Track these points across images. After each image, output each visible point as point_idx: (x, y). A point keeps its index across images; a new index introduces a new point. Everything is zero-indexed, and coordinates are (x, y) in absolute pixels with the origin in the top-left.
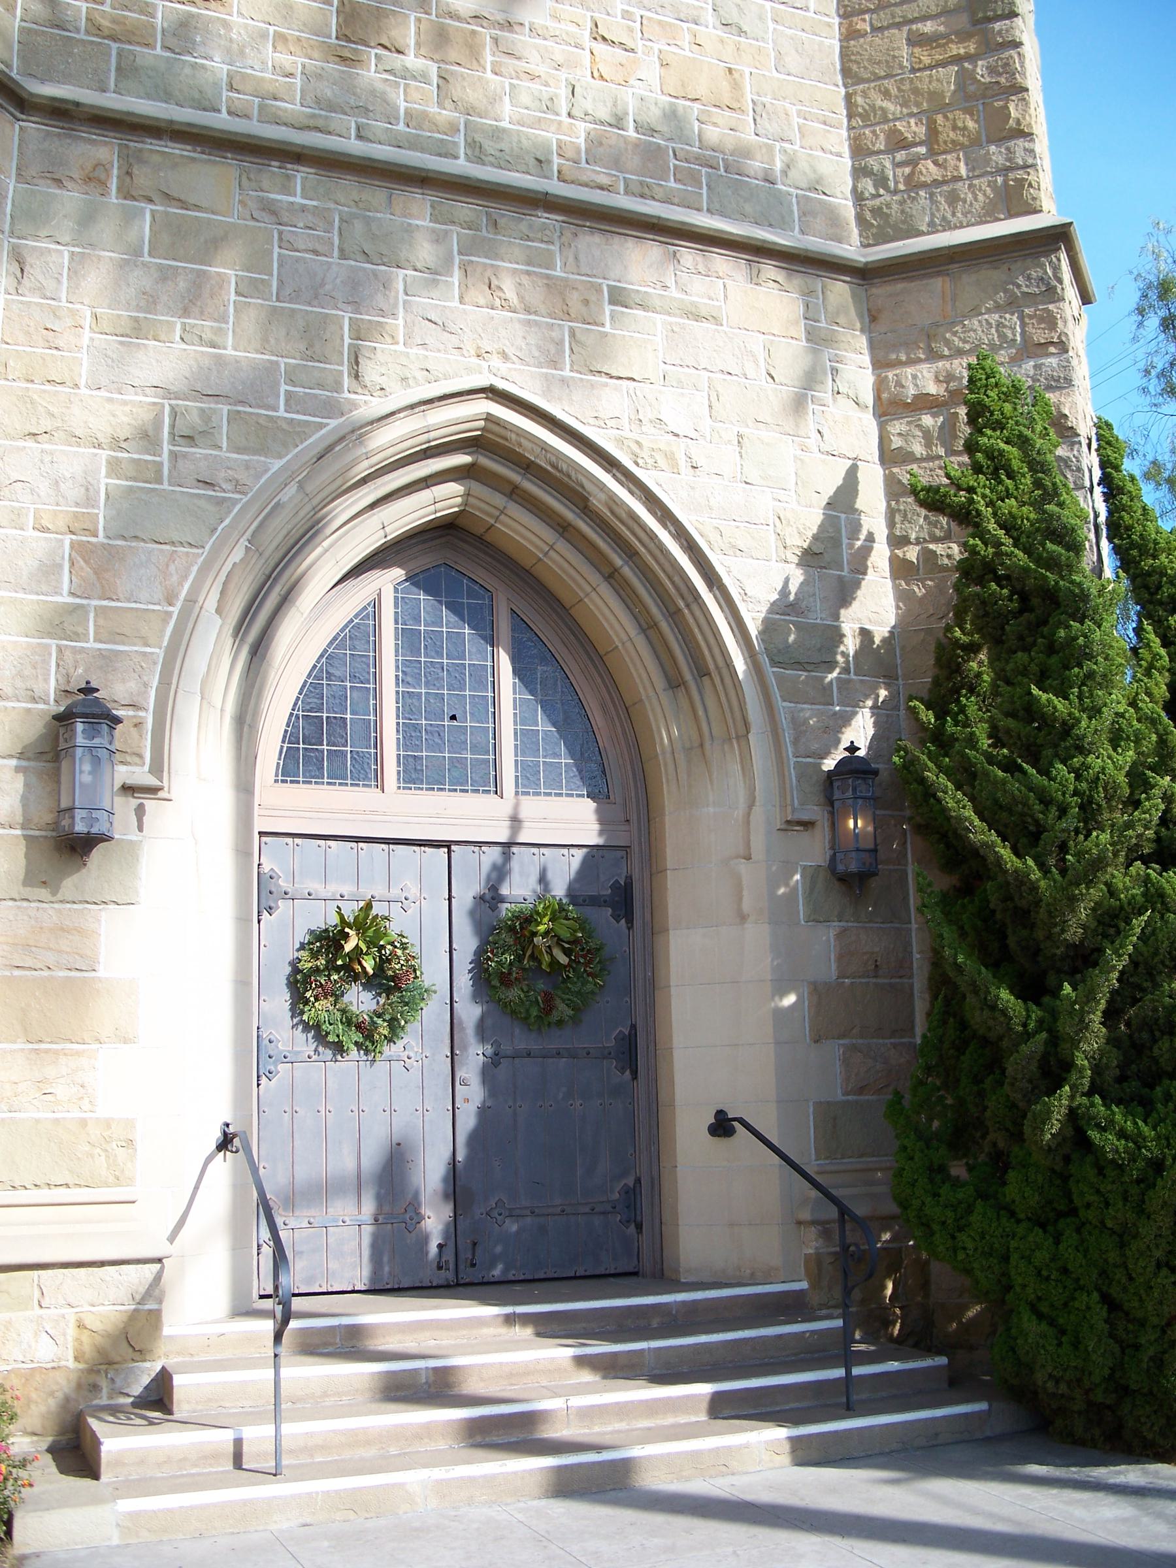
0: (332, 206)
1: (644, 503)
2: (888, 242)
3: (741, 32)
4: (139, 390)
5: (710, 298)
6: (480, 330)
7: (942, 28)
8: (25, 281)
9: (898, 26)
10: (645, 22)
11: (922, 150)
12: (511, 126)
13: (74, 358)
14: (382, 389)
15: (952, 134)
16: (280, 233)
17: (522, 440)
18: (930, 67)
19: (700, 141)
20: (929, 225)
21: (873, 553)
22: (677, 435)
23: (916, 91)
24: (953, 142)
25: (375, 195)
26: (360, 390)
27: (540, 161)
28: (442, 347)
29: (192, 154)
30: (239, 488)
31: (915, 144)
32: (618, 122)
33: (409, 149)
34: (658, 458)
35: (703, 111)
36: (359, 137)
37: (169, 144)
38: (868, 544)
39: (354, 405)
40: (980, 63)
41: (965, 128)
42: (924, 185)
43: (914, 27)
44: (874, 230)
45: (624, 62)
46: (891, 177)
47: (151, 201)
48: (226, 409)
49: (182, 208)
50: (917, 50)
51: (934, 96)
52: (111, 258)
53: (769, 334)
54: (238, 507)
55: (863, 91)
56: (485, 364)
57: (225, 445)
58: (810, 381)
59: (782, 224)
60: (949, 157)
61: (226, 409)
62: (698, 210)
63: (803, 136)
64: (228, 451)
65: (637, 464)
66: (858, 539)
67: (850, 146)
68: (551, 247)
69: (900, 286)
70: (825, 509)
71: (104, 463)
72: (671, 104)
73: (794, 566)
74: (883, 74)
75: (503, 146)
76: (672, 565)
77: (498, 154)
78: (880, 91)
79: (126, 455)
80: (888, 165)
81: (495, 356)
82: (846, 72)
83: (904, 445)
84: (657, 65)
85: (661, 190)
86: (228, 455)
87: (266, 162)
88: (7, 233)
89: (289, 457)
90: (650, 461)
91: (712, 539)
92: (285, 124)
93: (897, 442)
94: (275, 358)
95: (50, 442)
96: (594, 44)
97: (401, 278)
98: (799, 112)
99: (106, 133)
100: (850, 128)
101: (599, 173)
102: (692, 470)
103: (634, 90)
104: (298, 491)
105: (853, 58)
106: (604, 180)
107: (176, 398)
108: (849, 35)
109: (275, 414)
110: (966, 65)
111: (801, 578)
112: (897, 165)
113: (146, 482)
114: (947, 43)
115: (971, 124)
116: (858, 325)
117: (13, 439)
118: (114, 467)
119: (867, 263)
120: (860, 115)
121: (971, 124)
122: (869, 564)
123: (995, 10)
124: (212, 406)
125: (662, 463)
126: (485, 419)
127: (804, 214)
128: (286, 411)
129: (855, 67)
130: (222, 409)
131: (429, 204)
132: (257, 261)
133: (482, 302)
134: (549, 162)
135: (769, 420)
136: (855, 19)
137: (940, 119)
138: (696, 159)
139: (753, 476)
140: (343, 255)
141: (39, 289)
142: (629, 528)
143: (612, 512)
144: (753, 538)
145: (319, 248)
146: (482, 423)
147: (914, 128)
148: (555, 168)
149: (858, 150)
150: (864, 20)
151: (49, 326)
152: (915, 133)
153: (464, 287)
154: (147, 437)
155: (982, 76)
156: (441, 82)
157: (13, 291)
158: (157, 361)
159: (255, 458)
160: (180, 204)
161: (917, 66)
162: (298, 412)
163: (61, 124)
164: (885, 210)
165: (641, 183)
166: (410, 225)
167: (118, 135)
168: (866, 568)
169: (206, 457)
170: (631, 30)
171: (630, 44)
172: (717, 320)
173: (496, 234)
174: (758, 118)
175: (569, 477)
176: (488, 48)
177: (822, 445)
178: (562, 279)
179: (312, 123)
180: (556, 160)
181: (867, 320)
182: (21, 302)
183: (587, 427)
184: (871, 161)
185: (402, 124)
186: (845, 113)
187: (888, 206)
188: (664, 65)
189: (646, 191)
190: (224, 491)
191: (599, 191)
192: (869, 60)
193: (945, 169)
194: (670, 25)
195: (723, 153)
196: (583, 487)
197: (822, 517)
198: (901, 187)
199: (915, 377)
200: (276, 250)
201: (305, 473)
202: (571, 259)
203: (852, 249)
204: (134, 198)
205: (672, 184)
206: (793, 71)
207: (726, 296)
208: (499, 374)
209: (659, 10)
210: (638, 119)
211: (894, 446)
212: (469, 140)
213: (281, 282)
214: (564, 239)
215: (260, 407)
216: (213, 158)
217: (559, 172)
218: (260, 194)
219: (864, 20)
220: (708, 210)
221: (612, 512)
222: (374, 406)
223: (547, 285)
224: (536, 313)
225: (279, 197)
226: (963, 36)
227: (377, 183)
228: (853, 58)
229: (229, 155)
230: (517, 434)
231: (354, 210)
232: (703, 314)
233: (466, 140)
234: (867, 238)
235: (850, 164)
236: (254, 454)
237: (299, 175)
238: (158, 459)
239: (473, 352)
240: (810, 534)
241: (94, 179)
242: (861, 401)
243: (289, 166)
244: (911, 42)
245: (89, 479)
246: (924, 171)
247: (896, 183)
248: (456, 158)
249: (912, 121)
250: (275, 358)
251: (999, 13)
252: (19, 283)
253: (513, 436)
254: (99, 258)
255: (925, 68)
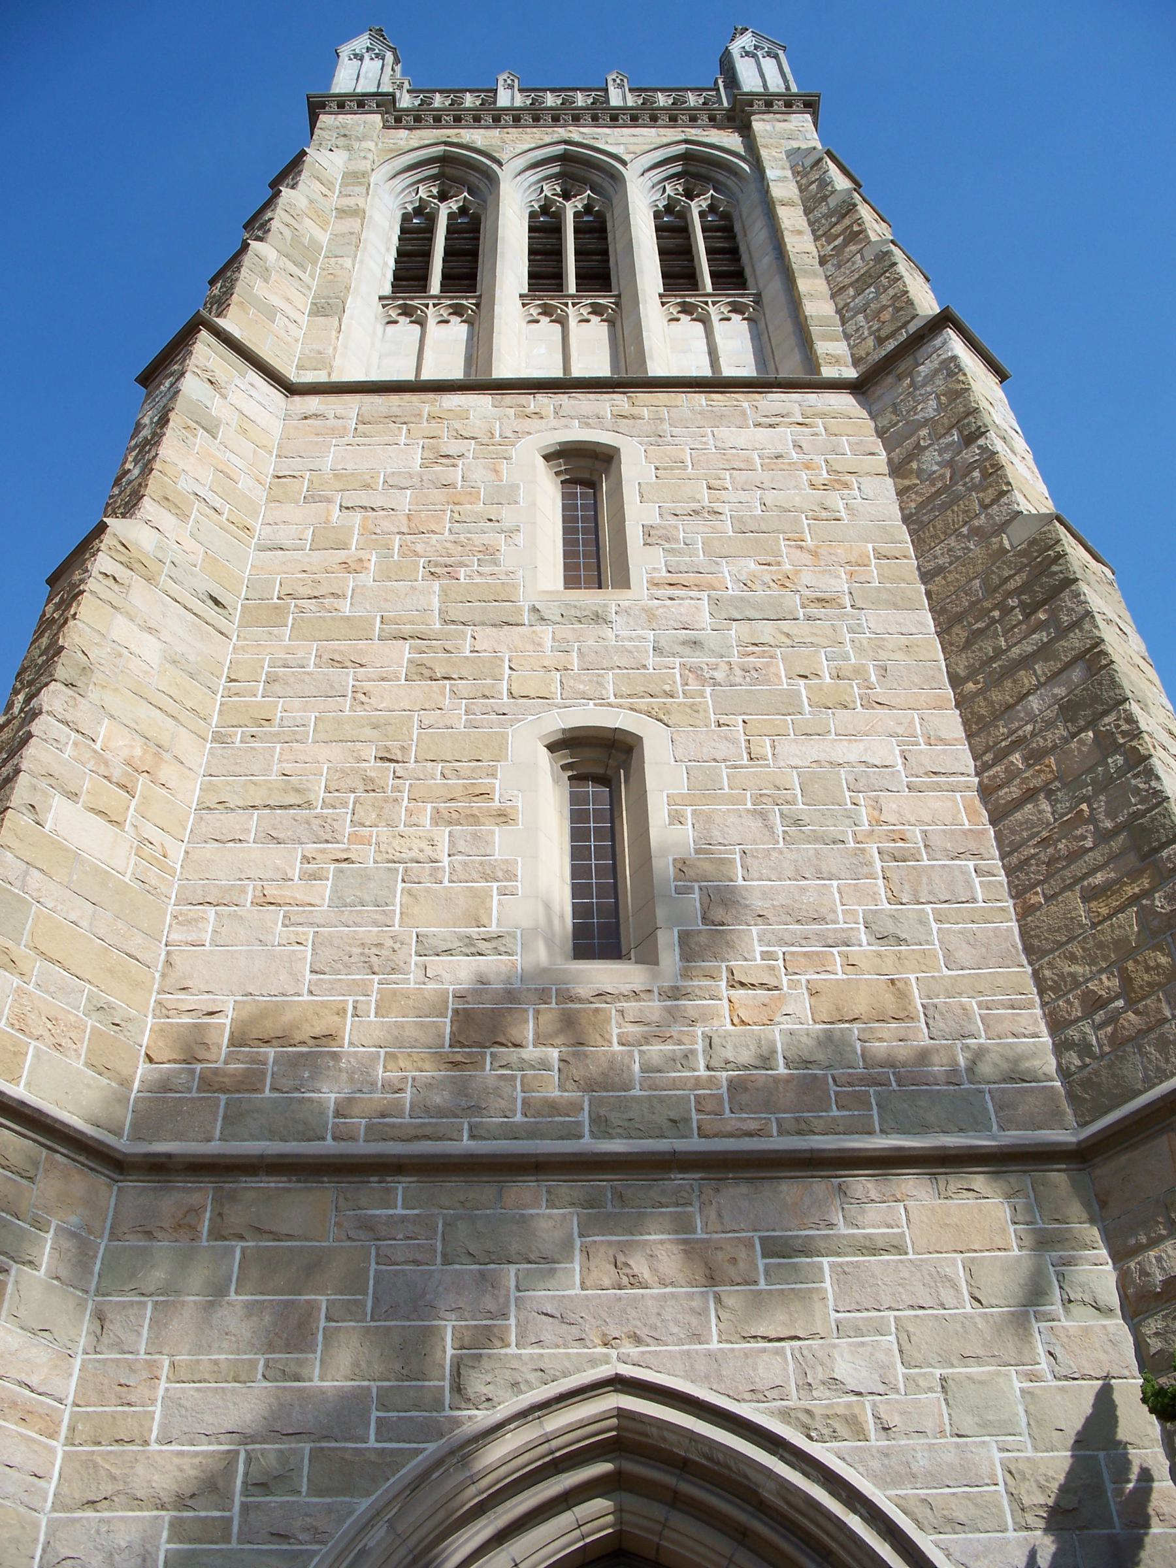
0: (436, 1211)
1: (823, 1486)
2: (1106, 1113)
3: (900, 941)
4: (213, 1439)
5: (889, 1226)
6: (604, 1315)
7: (1112, 875)
8: (105, 1339)
9: (1070, 887)
10: (787, 957)
11: (1120, 1003)
12: (643, 1093)
13: (146, 1412)
14: (489, 1400)
15: (1146, 977)
16: (378, 1248)
17: (666, 1434)
18: (1110, 917)
19: (864, 1060)
20: (1144, 1082)
21: (1154, 1495)
22: (859, 1394)
23: (1100, 945)
24: (1149, 984)
25: (482, 1191)
26: (463, 1405)
27: (674, 1121)
28: (560, 1341)
29: (287, 1185)
30: (318, 1536)
31: (1112, 1000)
32: (766, 1061)
33: (527, 1138)
34: (837, 1425)
35: (864, 1029)
36: (472, 1137)
37: (264, 1178)
38: (1144, 1484)
39: (457, 1422)
40: (1157, 895)
41: (1158, 966)
42: (1130, 1039)
43: (1085, 883)
44: (1089, 1105)
45: (767, 1001)
46: (1094, 1042)
47: (242, 1238)
48: (307, 1447)
49: (275, 1240)
50: (1093, 904)
51: (1120, 944)
52: (195, 1302)
53: (969, 1251)
54: (316, 1560)
55: (1049, 963)
56: (613, 1353)
57: (304, 1489)
58: (1033, 1297)
59: (979, 1124)
60: (1148, 1002)
61: (307, 1447)
62: (869, 1133)
63: (987, 1027)
64: (308, 1495)
65: (810, 1438)
66: (1129, 1481)
67: (1047, 1024)
68: (690, 1209)
69: (1124, 1158)
70: (1073, 1448)
71: (166, 1526)
72: (825, 1030)
73: (1039, 1533)
74: (1065, 939)
75: (631, 1115)
76: (855, 1542)
77: (626, 1124)
78: (1066, 957)
79: (191, 1514)
80: (1088, 1030)
81: (626, 1342)
82: (1028, 950)
83: (1166, 1347)
84: (806, 995)
85: (821, 1121)
86: (307, 1499)
87: (366, 1179)
88: (92, 1293)
89: (379, 1492)
90: (825, 1431)
91: (919, 1516)
92: (393, 1139)
93: (1155, 1345)
94: (366, 1383)
95: (110, 1509)
96: (732, 992)
97: (512, 1274)
98: (980, 1005)
99: (201, 1179)
100: (1044, 1005)
101: (745, 1119)
102: (883, 1433)
103: (782, 1026)
104: (388, 1531)
105: (1032, 933)
106: (752, 1126)
107: (253, 1443)
108: (1025, 912)
109: (364, 1445)
110: (1144, 902)
111: (1053, 1548)
112: (1097, 1028)
113: (211, 1543)
114: (1121, 888)
115: (1163, 960)
116: (1085, 1216)
117: (71, 1510)
118: (178, 1530)
119: (1079, 1143)
120: (1051, 988)
121: (1163, 960)
122: (1151, 1512)
123: (1158, 840)
124: (293, 1446)
125: (843, 1430)
126: (618, 1416)
127: (1001, 1108)
128: (377, 1441)
129: (1036, 942)
130: (303, 1449)
131: (544, 1190)
132: (354, 1282)
133: (607, 1282)
134: (687, 1120)
135: (980, 1352)
136: (1028, 895)
137: (1130, 965)
138: (861, 1080)
139: (967, 1423)
140: (447, 1261)
141: (117, 1344)
142: (812, 1521)
143: (788, 1503)
144: (976, 1505)
145: (419, 1257)
146: (615, 1421)
147: (1106, 983)
148: (695, 1125)
149: (1056, 1025)
150: (1037, 893)
151: (123, 1382)
152: (1108, 988)
153: (586, 1270)
154: (212, 1486)
155: (1162, 907)
156: (562, 1065)
157: (91, 1350)
158: (235, 1404)
159: (339, 1499)
160: (272, 1236)
161: (1096, 921)
162: (390, 1440)
163: (157, 1178)
164: (1095, 1080)
165: (796, 1119)
166: (523, 1215)
167: (213, 1179)
168: (1147, 1518)
169: (282, 1505)
170: (772, 968)
171: (773, 982)
172: (900, 1250)
173: (623, 1207)
174: (931, 1022)
175: (729, 1468)
176: (613, 1022)
177: (1057, 1368)
178: (703, 1240)
179: (420, 1132)
180: (694, 1116)
181: (1097, 1207)
182: (98, 1361)
183: (743, 1404)
184: (1073, 1033)
185: (519, 1115)
186: (1035, 990)
187: (1097, 1073)
188: (813, 993)
189: (803, 1126)
190: (301, 1543)
191: (747, 1139)
192: (1049, 930)
193: (1148, 1015)
194: (817, 953)
195: (893, 1066)
196: (747, 1477)
197: (1070, 1461)
198: (1107, 1049)
199: (1159, 1259)
200: (373, 1266)
201: (395, 1510)
202: (713, 1215)
203: (1065, 1135)
204: (225, 1238)
205: (835, 1112)
206: (968, 964)
207: (908, 1220)
208: (629, 1361)
209: (804, 942)
210: (788, 1054)
211: (1153, 1351)
212: (594, 1116)
213: (377, 1300)
214: (704, 1197)
215: (346, 1440)
216: (309, 1185)
217: (699, 1128)
218: (358, 1212)
219: (1037, 893)
220: (882, 1131)
221: (788, 1503)
222: (483, 1418)
223: (684, 1250)
224: (672, 1284)
225: (378, 1212)
226: (1134, 875)
227: (485, 1179)
228: (1032, 933)
229: (326, 1179)
230: (658, 1428)
231: (461, 1211)
232: (880, 1245)
233: (590, 1117)
234: (1083, 1115)
235: (1050, 1041)
236: (337, 1496)
237: (400, 1186)
238: (227, 1514)
239: (597, 1341)
240: (1055, 1486)
241: (185, 1226)
242: (1101, 1304)
243: (389, 1179)
244: (1085, 899)
245: (148, 1546)
246: (1126, 1024)
247: (1101, 1046)
248: (581, 1137)
249: (1104, 977)
250: (366, 1383)
251: (1164, 840)
252: (98, 1340)
253: (654, 1431)
254: (183, 1303)
255: (1105, 919)
